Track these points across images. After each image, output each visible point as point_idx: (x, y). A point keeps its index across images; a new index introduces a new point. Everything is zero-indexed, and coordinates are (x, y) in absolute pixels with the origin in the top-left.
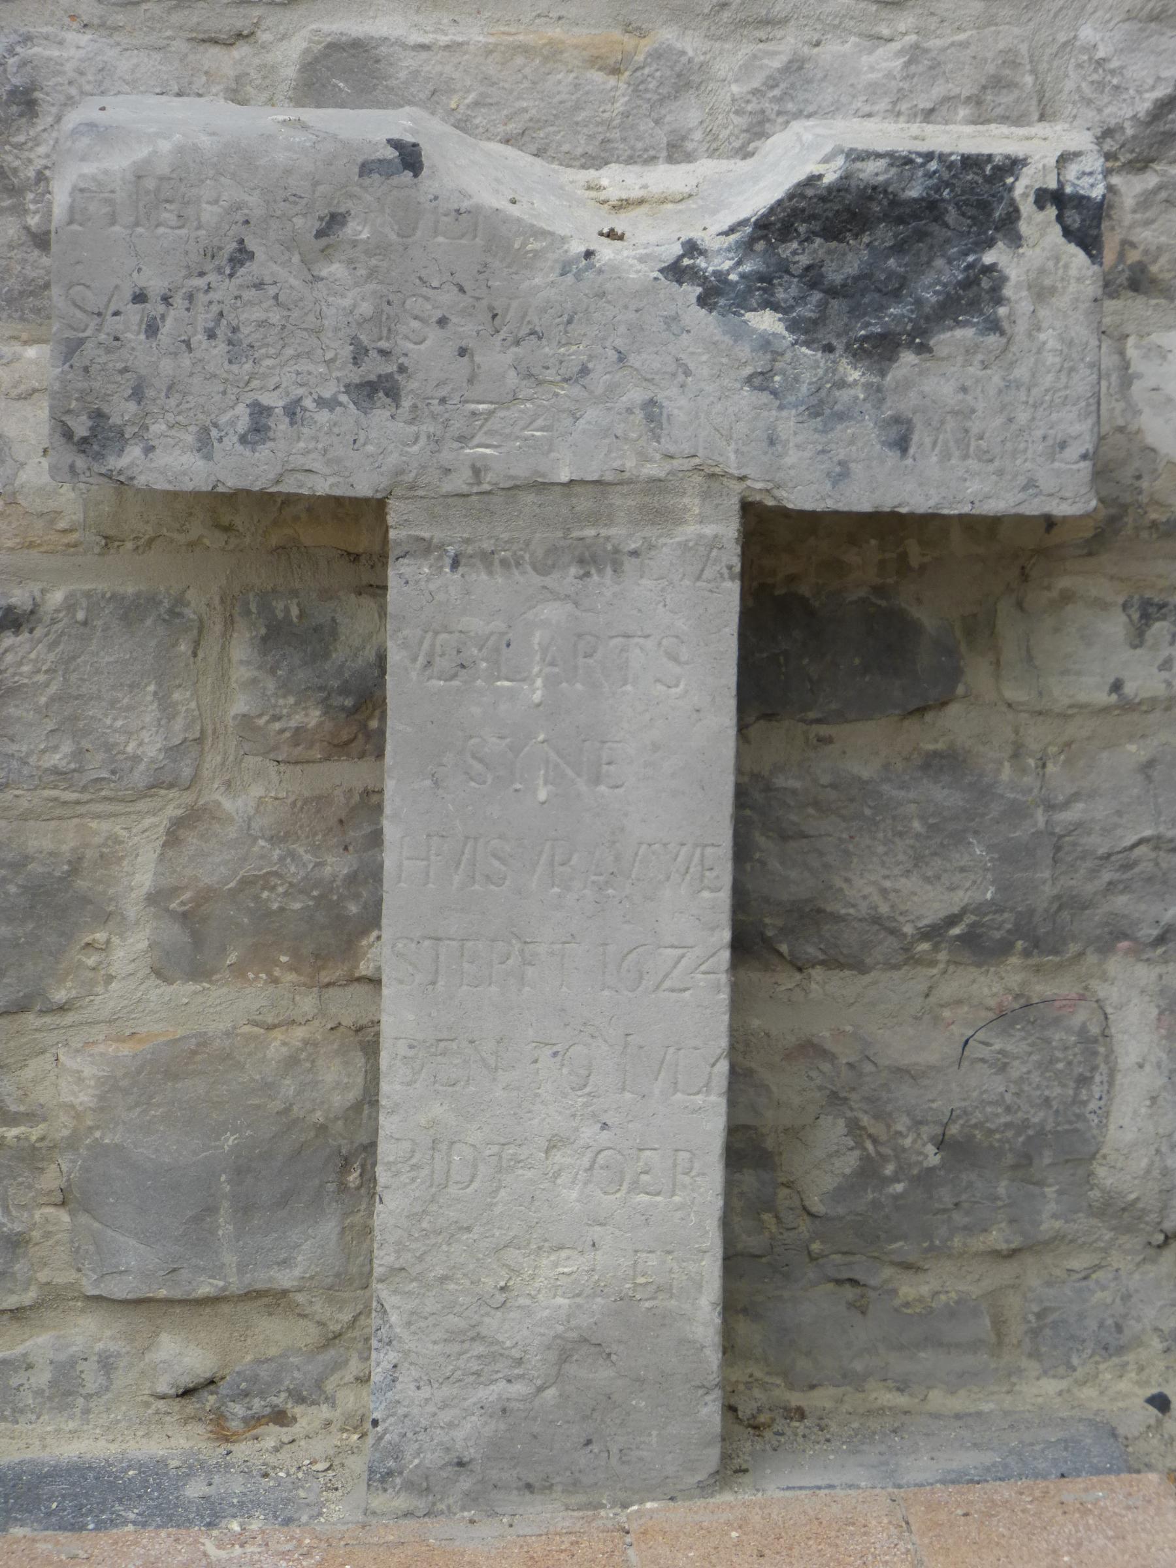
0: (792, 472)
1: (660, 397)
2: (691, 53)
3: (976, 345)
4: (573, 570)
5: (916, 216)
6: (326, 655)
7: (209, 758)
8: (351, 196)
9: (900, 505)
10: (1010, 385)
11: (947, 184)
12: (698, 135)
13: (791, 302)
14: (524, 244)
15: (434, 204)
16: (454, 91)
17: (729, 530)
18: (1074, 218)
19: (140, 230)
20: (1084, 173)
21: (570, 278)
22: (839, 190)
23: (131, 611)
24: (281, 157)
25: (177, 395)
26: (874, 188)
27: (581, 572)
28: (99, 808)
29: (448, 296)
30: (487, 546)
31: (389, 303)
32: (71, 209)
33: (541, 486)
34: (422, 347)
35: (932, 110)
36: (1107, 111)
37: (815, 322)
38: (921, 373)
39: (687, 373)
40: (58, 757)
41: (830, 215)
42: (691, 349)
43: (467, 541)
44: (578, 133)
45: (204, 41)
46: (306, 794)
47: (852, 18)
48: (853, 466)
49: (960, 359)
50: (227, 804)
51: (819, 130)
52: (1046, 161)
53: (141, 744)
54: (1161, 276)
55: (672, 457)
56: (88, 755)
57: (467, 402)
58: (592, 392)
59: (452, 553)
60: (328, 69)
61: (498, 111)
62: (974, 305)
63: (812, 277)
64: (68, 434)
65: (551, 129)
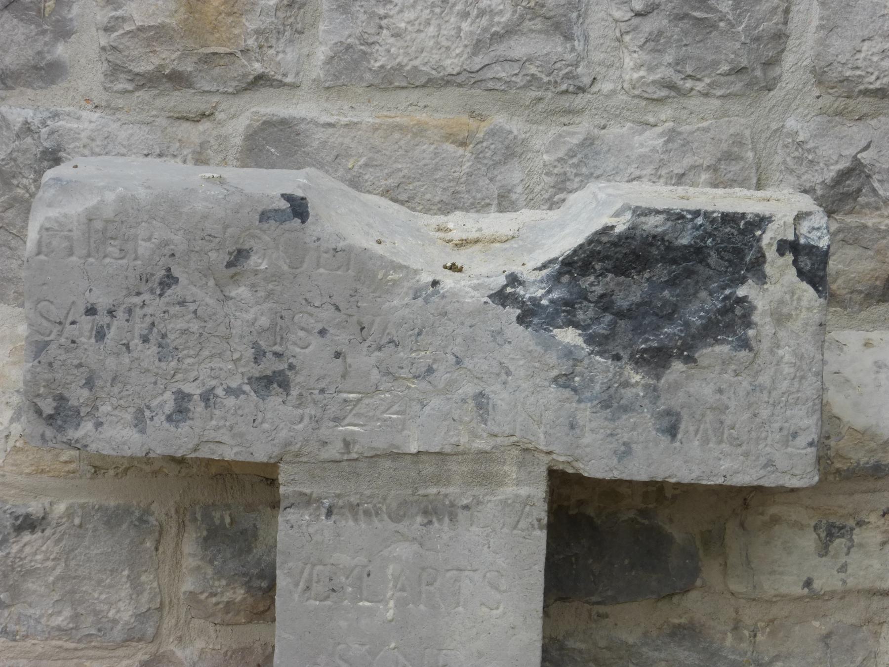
0: (588, 450)
1: (488, 391)
2: (516, 132)
3: (731, 358)
4: (419, 519)
5: (686, 259)
6: (249, 550)
7: (166, 621)
8: (254, 237)
9: (669, 477)
10: (756, 388)
11: (710, 235)
12: (519, 189)
13: (589, 321)
14: (385, 275)
15: (317, 244)
16: (351, 156)
17: (538, 491)
18: (806, 263)
19: (91, 260)
20: (813, 229)
21: (420, 302)
22: (627, 238)
23: (113, 519)
24: (200, 206)
25: (119, 385)
26: (654, 237)
27: (426, 521)
28: (91, 653)
29: (327, 314)
30: (354, 499)
31: (282, 318)
32: (39, 243)
33: (395, 456)
34: (307, 351)
35: (683, 175)
36: (804, 178)
37: (606, 337)
38: (687, 378)
39: (508, 373)
40: (61, 619)
41: (620, 256)
42: (511, 356)
43: (338, 496)
44: (437, 186)
45: (178, 118)
46: (234, 646)
47: (628, 110)
48: (634, 446)
49: (718, 368)
50: (179, 653)
51: (610, 191)
52: (786, 219)
53: (118, 611)
54: (838, 292)
55: (495, 436)
56: (82, 618)
57: (340, 392)
58: (435, 387)
59: (327, 505)
60: (264, 139)
61: (382, 170)
62: (729, 328)
63: (605, 303)
64: (39, 412)
65: (418, 183)
